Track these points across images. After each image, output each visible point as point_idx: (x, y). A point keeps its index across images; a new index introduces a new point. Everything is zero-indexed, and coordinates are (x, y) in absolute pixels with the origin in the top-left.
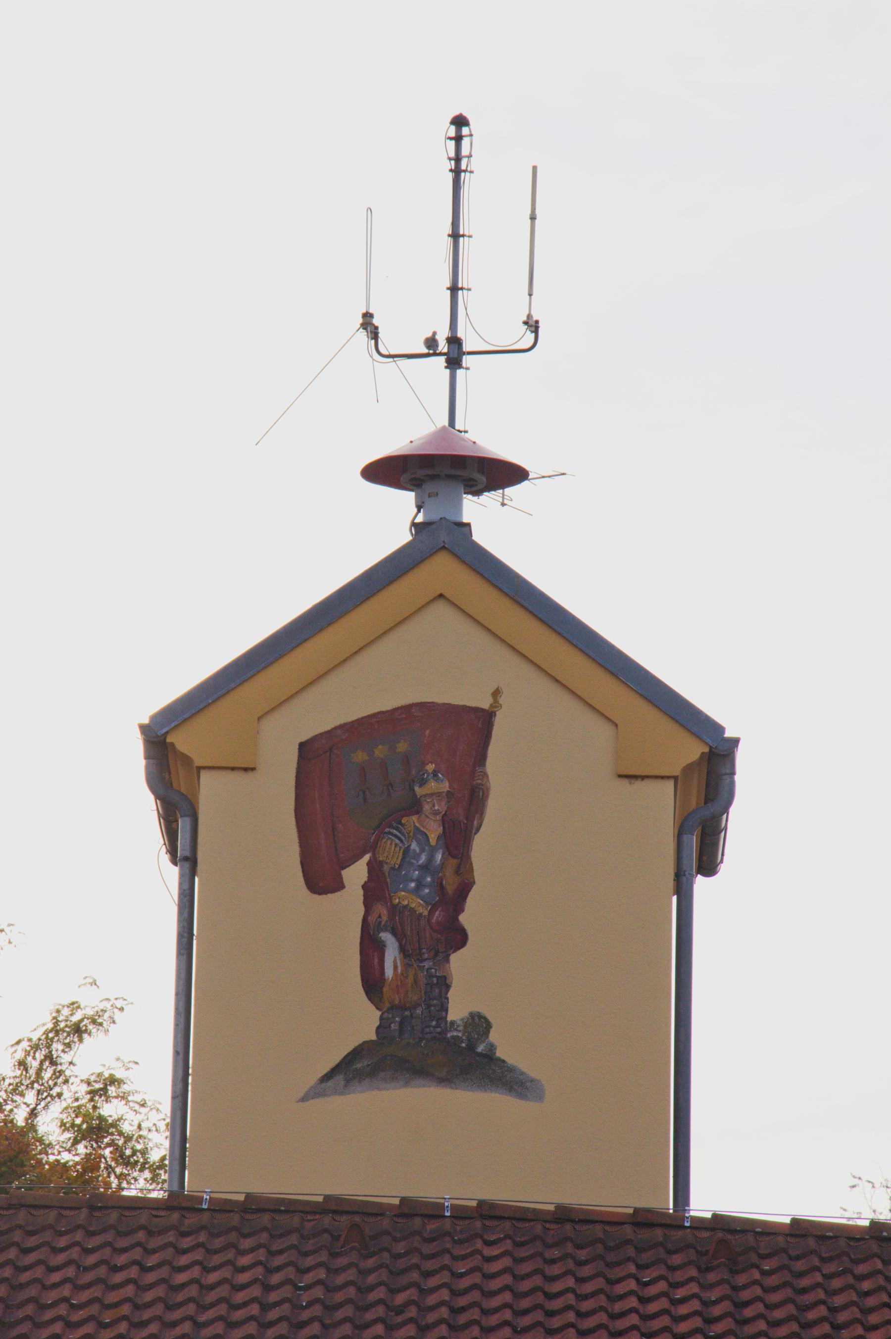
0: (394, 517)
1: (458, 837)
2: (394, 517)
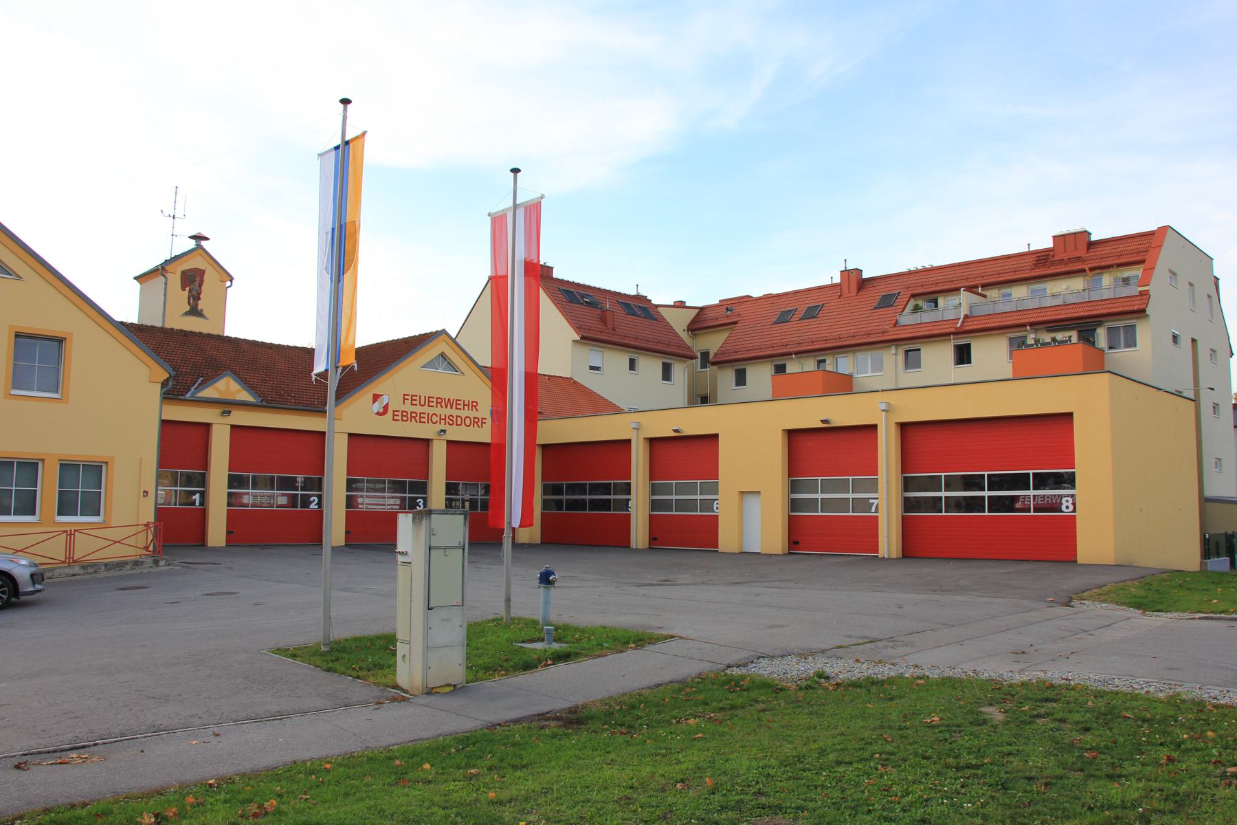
0: (192, 244)
1: (200, 286)
2: (192, 244)
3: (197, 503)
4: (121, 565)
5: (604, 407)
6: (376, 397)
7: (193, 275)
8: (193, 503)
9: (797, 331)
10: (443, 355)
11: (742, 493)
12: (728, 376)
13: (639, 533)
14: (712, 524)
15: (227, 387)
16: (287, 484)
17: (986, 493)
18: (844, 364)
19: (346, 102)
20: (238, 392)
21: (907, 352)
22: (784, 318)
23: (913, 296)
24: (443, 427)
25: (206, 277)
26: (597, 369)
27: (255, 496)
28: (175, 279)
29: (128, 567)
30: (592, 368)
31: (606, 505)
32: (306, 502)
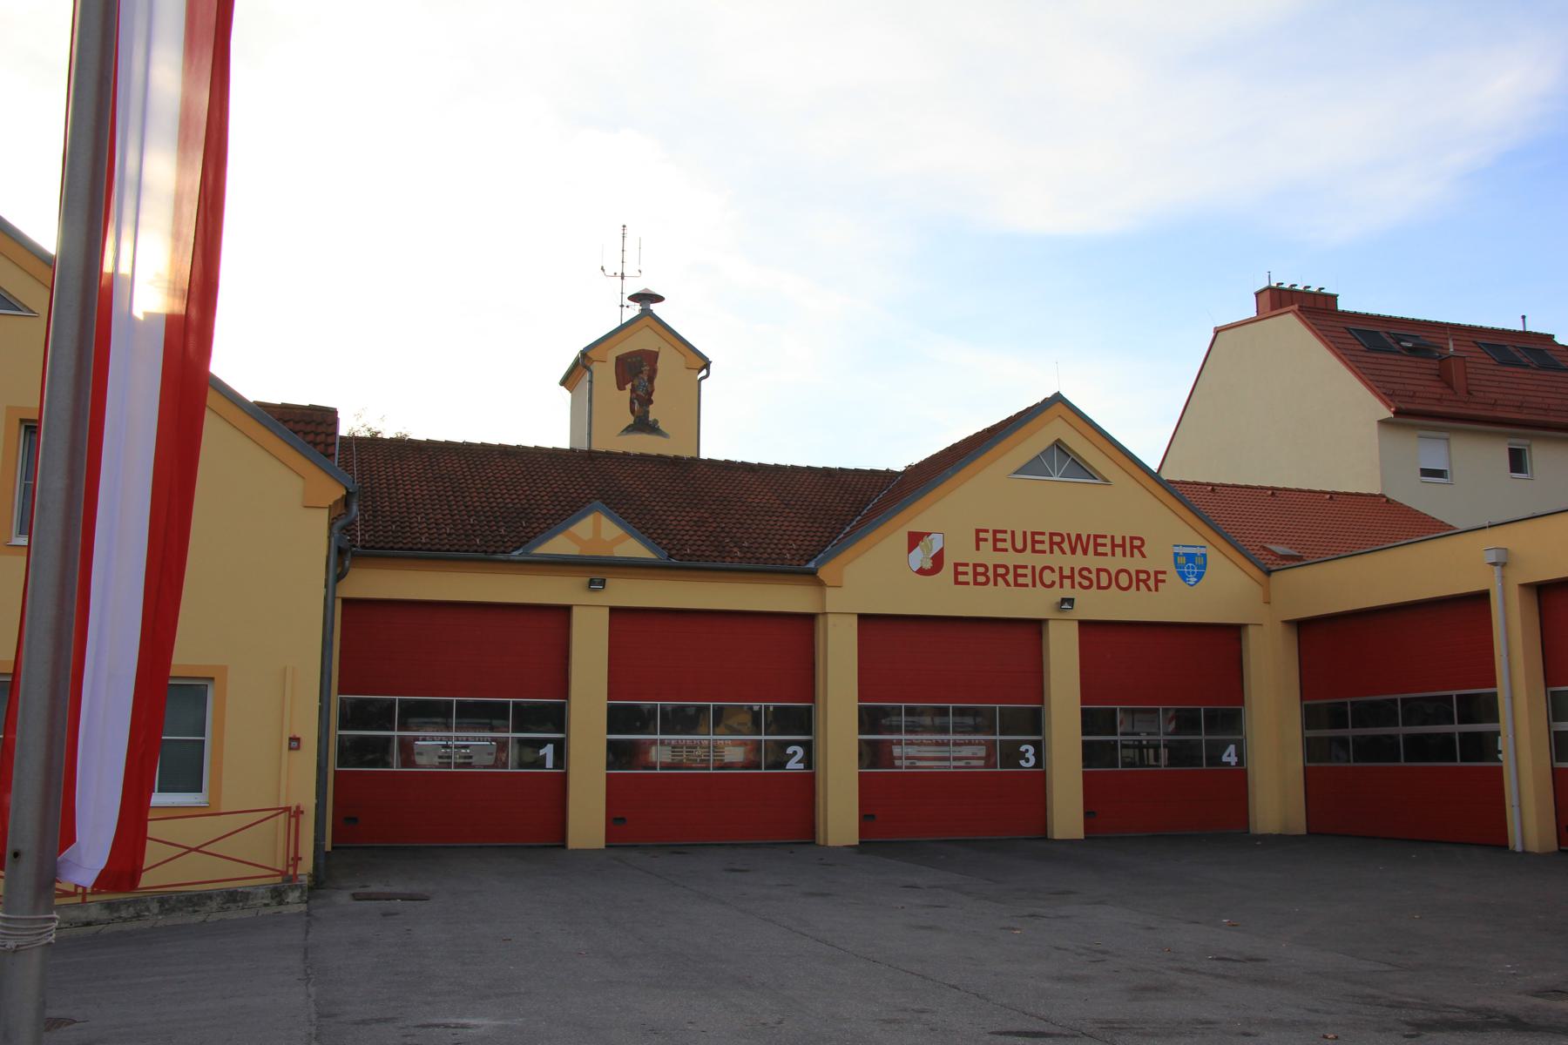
0: (635, 309)
1: (651, 379)
2: (635, 309)
3: (549, 763)
4: (195, 901)
5: (1425, 528)
6: (915, 539)
7: (639, 364)
8: (540, 762)
10: (1059, 445)
15: (596, 532)
16: (979, 722)
20: (618, 541)
24: (1067, 592)
25: (660, 364)
26: (1439, 473)
27: (675, 747)
28: (605, 373)
29: (214, 905)
30: (1426, 472)
31: (1442, 749)
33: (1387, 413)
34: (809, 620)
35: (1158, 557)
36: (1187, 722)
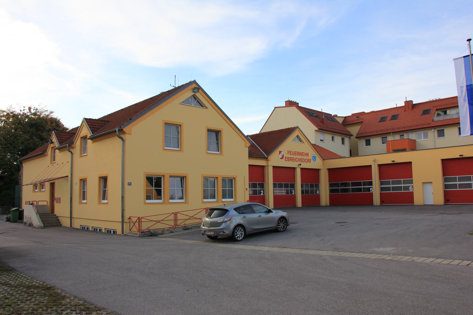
9: (388, 125)
10: (298, 137)
11: (423, 183)
12: (363, 142)
13: (377, 200)
14: (411, 195)
17: (402, 185)
18: (412, 136)
19: (469, 40)
21: (438, 131)
22: (383, 119)
23: (437, 110)
24: (300, 163)
32: (291, 192)
33: (317, 129)
34: (263, 167)
35: (310, 157)
36: (312, 186)
